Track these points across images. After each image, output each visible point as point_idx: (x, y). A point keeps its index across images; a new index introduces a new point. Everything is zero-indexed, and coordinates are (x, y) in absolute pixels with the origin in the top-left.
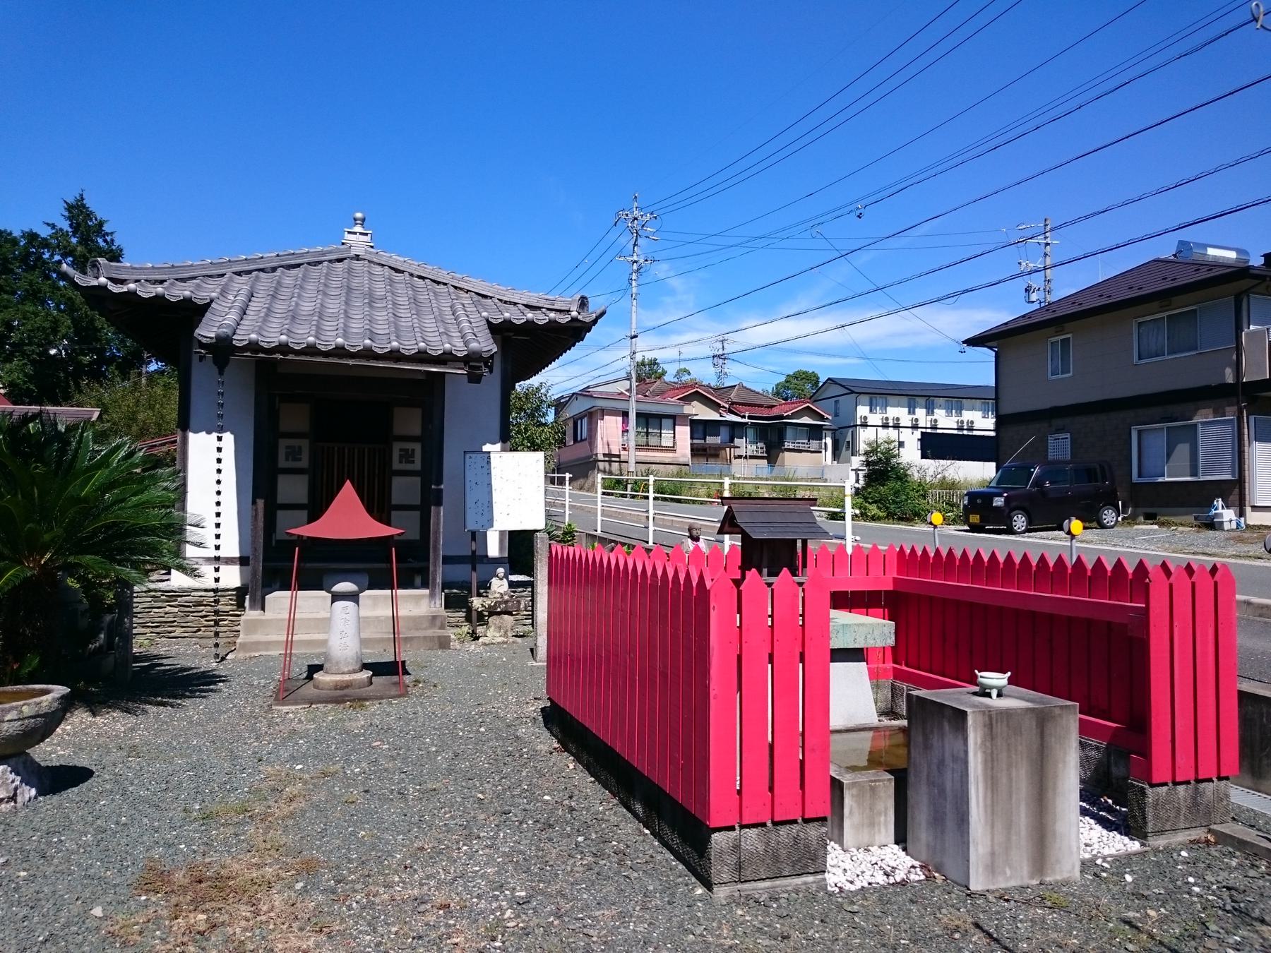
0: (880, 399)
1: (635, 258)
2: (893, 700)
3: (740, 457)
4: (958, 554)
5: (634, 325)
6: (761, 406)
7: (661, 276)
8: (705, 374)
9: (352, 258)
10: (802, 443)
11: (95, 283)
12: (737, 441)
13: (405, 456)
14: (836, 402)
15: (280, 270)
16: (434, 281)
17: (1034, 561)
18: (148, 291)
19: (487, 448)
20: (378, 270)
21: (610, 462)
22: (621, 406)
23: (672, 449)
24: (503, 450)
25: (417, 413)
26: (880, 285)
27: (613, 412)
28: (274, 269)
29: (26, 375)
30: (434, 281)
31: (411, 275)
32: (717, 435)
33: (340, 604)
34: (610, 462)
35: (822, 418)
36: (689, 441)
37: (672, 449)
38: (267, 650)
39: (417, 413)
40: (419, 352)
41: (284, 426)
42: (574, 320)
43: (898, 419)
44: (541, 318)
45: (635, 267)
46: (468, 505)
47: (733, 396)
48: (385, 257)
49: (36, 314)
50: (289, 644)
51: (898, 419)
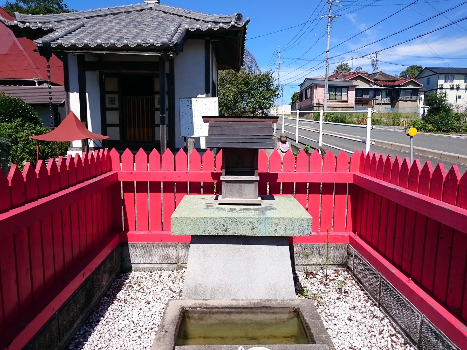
0: (450, 76)
1: (330, 16)
2: (348, 258)
3: (378, 104)
4: (393, 160)
5: (328, 47)
6: (390, 81)
7: (362, 29)
9: (148, 9)
10: (408, 97)
14: (429, 78)
17: (445, 172)
21: (319, 107)
23: (346, 101)
24: (207, 97)
26: (441, 12)
30: (178, 15)
32: (368, 94)
34: (319, 107)
35: (419, 86)
36: (354, 97)
37: (346, 101)
42: (233, 26)
43: (459, 85)
44: (216, 27)
45: (330, 19)
46: (181, 125)
47: (377, 77)
51: (459, 85)
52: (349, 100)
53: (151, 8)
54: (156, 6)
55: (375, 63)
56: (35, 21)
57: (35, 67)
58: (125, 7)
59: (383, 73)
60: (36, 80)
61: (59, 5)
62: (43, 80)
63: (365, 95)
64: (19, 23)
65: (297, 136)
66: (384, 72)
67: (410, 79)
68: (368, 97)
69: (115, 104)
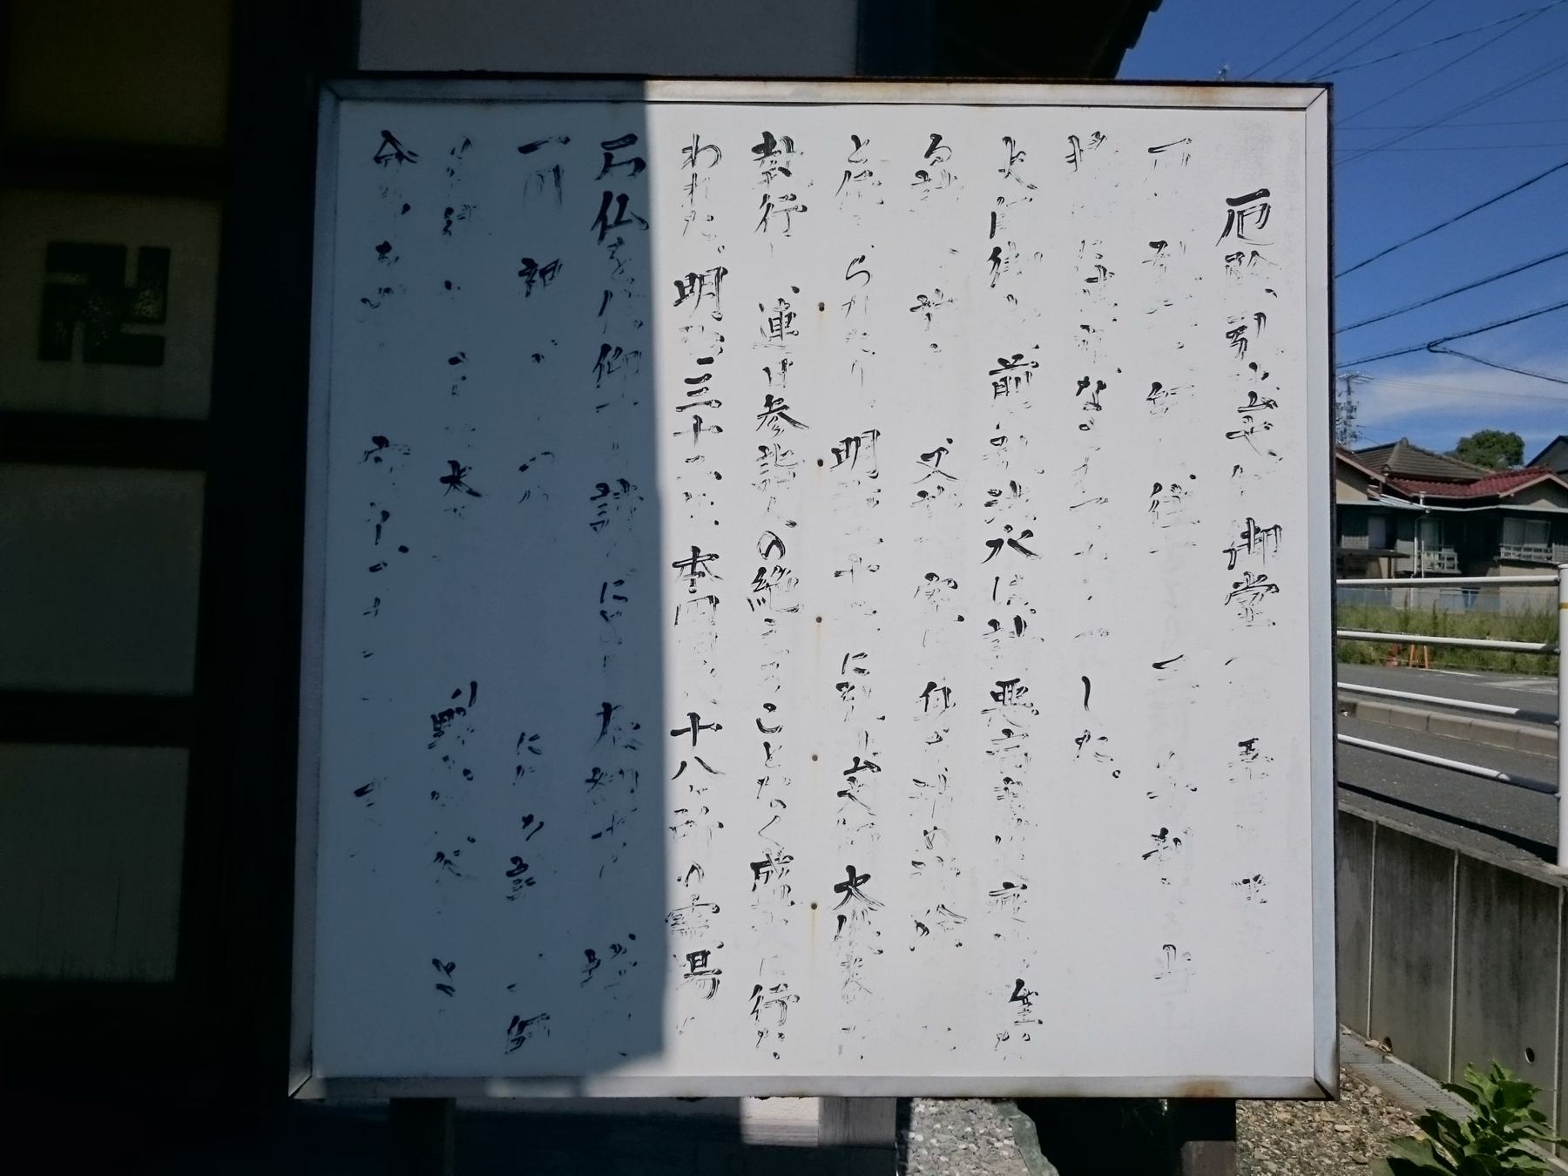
6: (1447, 480)
10: (1536, 549)
12: (1402, 546)
32: (1362, 532)
47: (1392, 461)
63: (1348, 535)
67: (1541, 473)
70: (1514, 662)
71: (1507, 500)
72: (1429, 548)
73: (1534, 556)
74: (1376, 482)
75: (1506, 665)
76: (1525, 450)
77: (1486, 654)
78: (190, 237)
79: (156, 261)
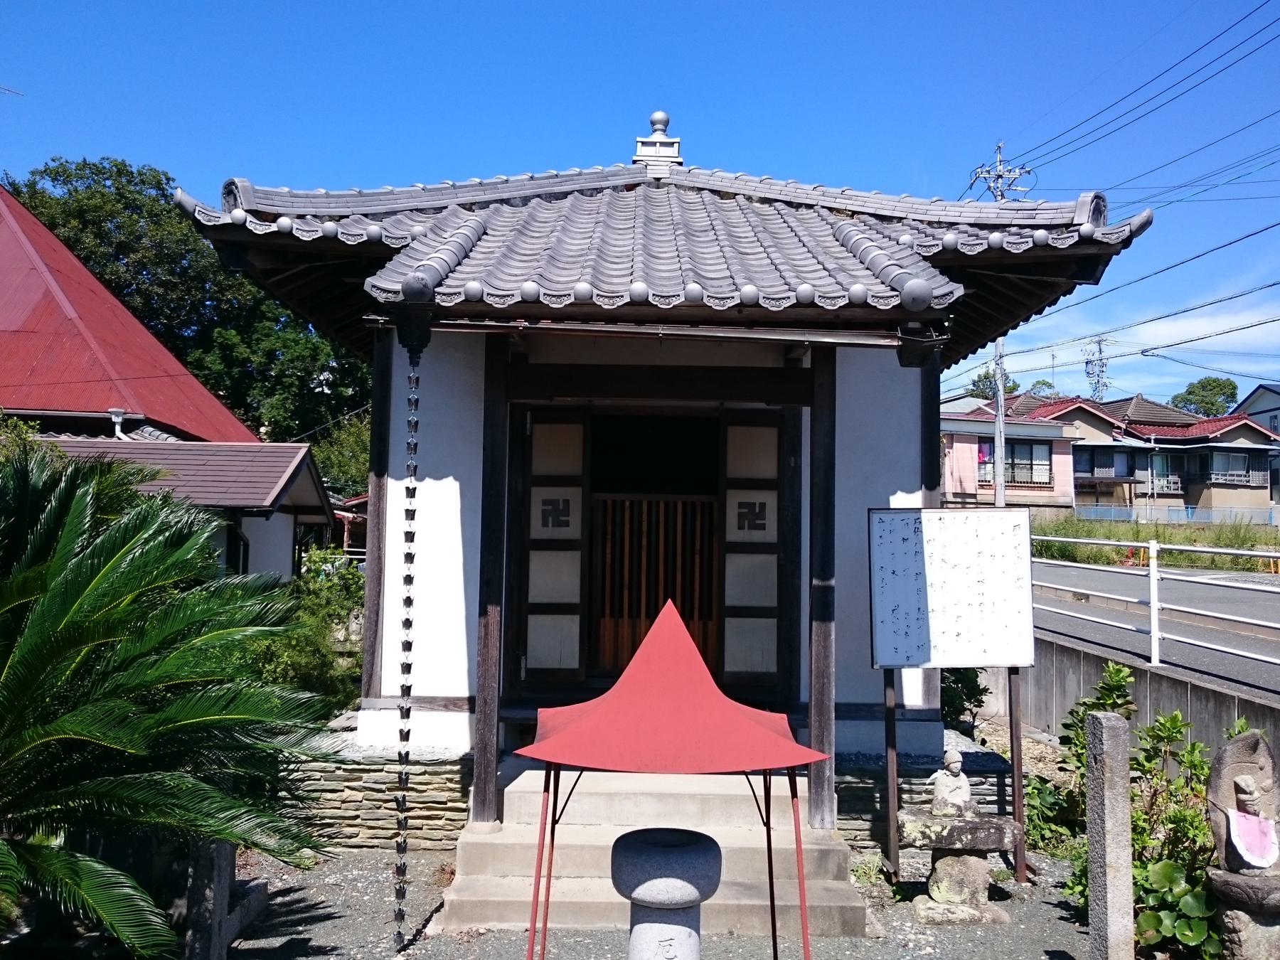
3: (1144, 495)
8: (1077, 386)
9: (649, 184)
10: (1237, 475)
11: (226, 219)
12: (1139, 474)
13: (748, 516)
15: (534, 201)
16: (789, 204)
18: (306, 233)
19: (900, 500)
20: (692, 196)
22: (983, 429)
23: (1048, 486)
25: (768, 437)
27: (966, 438)
28: (526, 201)
29: (286, 410)
30: (789, 204)
31: (749, 198)
33: (651, 933)
35: (1267, 440)
37: (1048, 486)
38: (501, 919)
39: (768, 437)
40: (799, 304)
41: (542, 464)
44: (1017, 245)
47: (1131, 412)
48: (703, 177)
49: (296, 342)
50: (540, 907)
52: (1057, 483)
53: (658, 179)
54: (678, 173)
55: (1097, 369)
56: (302, 211)
57: (114, 375)
58: (580, 174)
59: (1146, 401)
60: (117, 414)
61: (163, 190)
62: (141, 416)
64: (250, 218)
65: (1156, 634)
66: (1151, 399)
68: (1110, 473)
69: (567, 524)
70: (1213, 561)
71: (1215, 440)
72: (1158, 475)
73: (1236, 480)
74: (1119, 428)
75: (1208, 563)
76: (1238, 392)
77: (1193, 556)
78: (769, 499)
79: (763, 505)
